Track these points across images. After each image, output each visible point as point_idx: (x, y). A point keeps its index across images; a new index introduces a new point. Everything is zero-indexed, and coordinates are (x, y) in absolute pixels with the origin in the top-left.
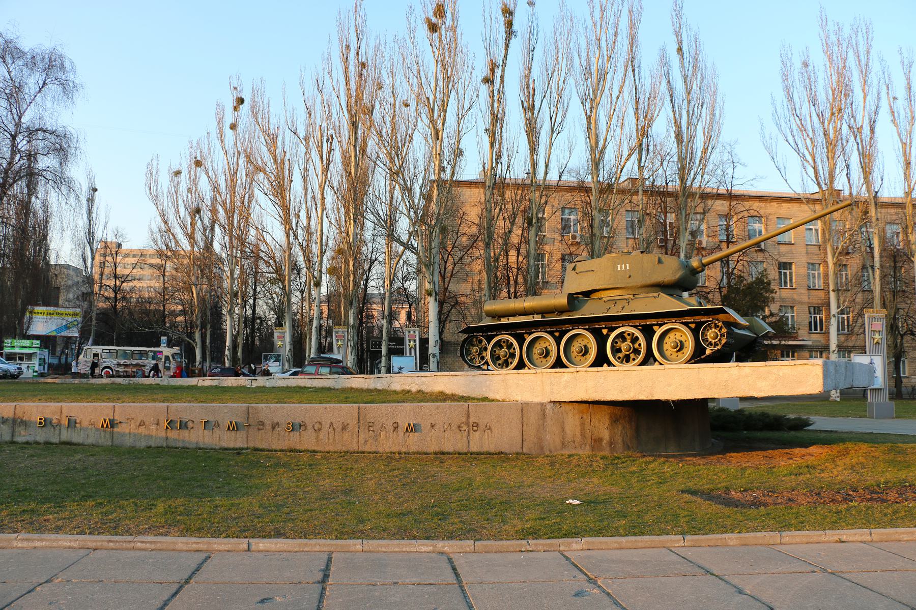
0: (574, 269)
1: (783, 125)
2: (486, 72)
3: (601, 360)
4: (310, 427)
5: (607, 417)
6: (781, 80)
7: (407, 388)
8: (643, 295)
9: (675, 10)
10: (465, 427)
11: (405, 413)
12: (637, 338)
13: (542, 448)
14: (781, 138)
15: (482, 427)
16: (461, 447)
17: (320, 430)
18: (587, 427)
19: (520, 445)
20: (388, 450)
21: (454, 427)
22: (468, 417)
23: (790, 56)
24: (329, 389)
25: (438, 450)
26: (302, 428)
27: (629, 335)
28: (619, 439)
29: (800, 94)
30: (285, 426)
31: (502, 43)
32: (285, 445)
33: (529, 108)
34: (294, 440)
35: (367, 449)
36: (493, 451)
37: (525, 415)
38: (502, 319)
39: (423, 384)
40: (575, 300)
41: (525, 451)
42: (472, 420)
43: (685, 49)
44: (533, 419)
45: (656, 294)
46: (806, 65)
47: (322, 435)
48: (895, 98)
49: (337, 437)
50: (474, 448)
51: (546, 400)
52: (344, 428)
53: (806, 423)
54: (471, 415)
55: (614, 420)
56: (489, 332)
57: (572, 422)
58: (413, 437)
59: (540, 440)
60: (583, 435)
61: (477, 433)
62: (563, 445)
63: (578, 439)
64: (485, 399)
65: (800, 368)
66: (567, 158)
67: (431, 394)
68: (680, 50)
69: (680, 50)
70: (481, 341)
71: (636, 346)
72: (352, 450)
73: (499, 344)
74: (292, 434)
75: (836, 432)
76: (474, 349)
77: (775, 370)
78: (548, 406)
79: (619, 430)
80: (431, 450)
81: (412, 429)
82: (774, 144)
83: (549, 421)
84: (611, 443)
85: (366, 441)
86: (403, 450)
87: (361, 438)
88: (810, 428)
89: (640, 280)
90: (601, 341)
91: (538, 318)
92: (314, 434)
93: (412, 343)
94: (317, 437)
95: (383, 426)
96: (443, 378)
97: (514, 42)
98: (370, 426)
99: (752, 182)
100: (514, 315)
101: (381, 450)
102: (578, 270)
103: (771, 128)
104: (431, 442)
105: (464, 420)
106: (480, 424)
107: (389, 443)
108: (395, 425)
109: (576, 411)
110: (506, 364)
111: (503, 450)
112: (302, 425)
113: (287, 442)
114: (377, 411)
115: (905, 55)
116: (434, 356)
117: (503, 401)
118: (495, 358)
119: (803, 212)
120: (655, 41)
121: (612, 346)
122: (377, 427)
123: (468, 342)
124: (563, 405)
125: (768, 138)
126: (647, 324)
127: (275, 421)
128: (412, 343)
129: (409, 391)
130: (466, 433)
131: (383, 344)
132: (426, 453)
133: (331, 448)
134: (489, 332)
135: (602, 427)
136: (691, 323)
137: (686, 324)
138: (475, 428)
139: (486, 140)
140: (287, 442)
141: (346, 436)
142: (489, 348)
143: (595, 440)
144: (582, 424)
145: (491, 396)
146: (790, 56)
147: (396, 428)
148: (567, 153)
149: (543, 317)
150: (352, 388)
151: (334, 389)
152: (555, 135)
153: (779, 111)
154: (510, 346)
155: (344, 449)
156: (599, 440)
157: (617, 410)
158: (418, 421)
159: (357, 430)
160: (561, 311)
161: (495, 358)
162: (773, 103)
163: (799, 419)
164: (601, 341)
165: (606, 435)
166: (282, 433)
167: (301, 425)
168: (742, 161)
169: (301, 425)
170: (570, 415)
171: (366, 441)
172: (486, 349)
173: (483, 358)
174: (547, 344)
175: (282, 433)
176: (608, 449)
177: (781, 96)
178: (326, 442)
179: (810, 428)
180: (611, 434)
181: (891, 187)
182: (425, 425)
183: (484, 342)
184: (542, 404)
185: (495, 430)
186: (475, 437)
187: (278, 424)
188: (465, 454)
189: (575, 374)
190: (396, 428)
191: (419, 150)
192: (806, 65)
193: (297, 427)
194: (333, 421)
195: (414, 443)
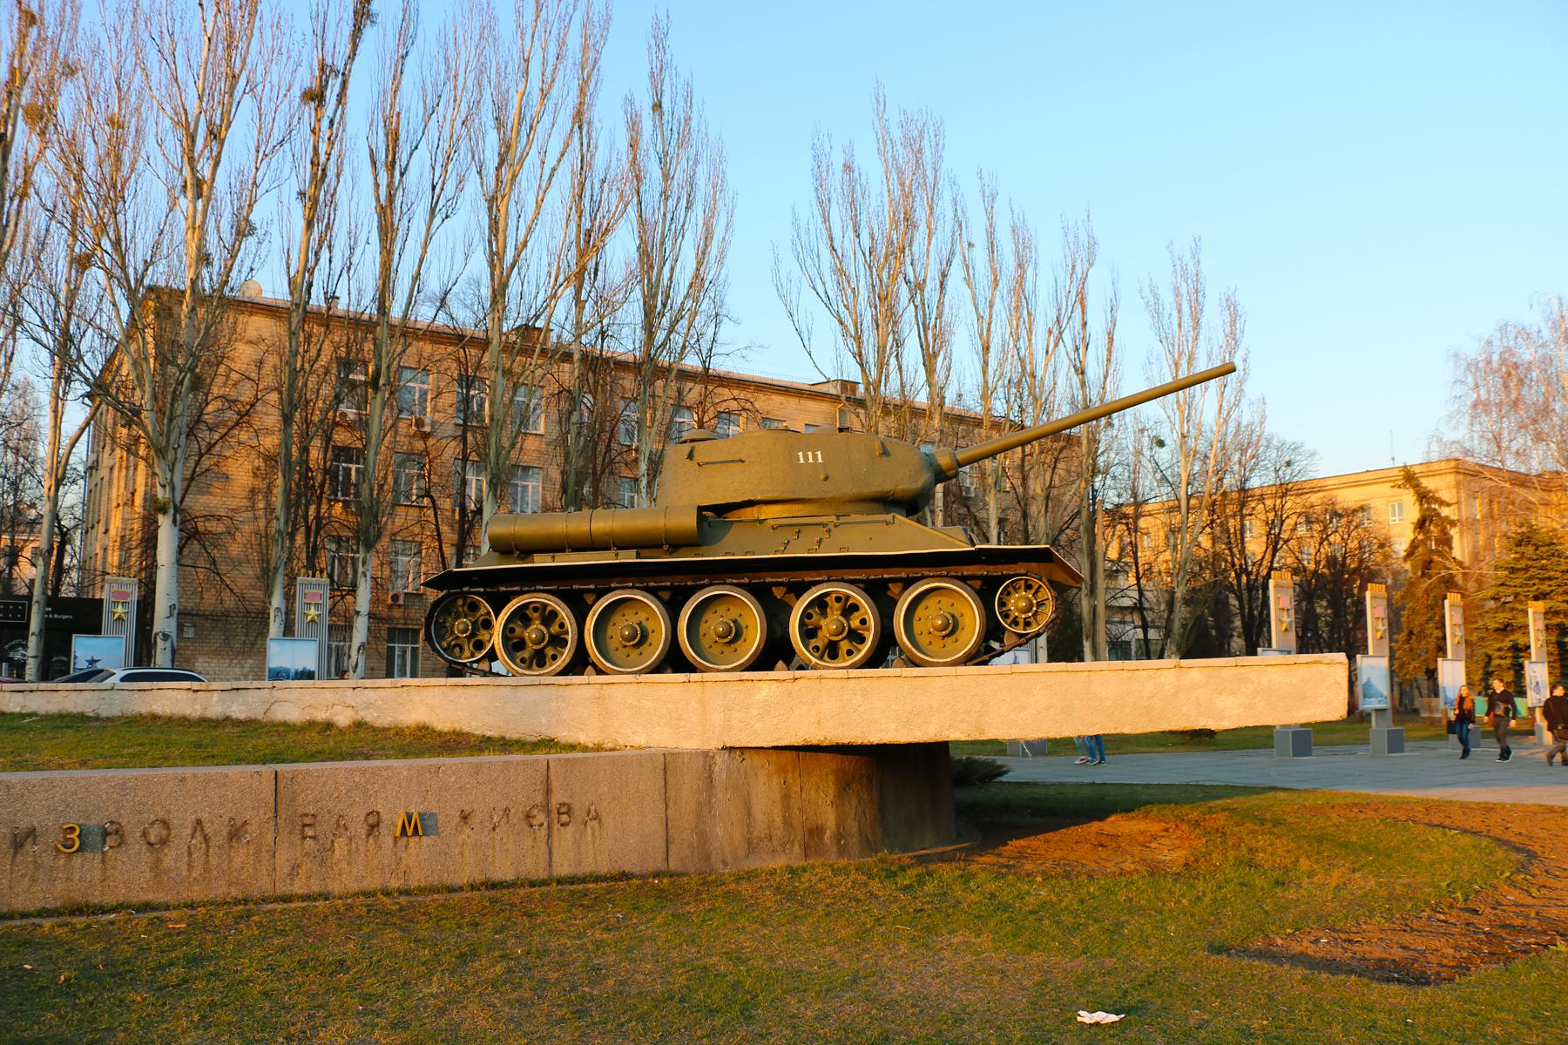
0: (690, 456)
1: (809, 262)
2: (306, 78)
3: (775, 653)
4: (134, 836)
5: (831, 778)
6: (812, 188)
7: (321, 716)
8: (854, 517)
9: (655, 37)
10: (541, 817)
11: (398, 785)
12: (855, 608)
13: (708, 857)
14: (806, 283)
15: (579, 814)
16: (533, 866)
17: (164, 842)
18: (795, 804)
19: (661, 855)
20: (354, 887)
21: (517, 818)
22: (548, 791)
23: (827, 149)
24: (82, 718)
25: (480, 878)
26: (111, 841)
27: (838, 599)
28: (852, 826)
29: (837, 215)
30: (55, 838)
31: (347, 30)
32: (53, 893)
33: (390, 161)
34: (84, 878)
35: (298, 888)
36: (604, 871)
37: (671, 781)
38: (537, 557)
39: (369, 705)
40: (716, 516)
41: (672, 866)
42: (557, 798)
43: (666, 105)
44: (687, 785)
45: (889, 517)
46: (848, 168)
47: (169, 858)
48: (970, 245)
49: (214, 861)
50: (563, 868)
51: (713, 744)
52: (235, 834)
53: (1000, 771)
54: (555, 785)
55: (844, 786)
56: (497, 587)
57: (765, 790)
58: (419, 848)
59: (704, 838)
60: (787, 822)
61: (570, 830)
62: (751, 847)
63: (778, 832)
64: (549, 744)
65: (1303, 669)
66: (446, 273)
67: (399, 732)
68: (657, 106)
69: (657, 106)
70: (474, 607)
71: (855, 623)
72: (257, 894)
73: (521, 615)
74: (77, 861)
75: (1035, 784)
76: (461, 625)
77: (1253, 674)
78: (718, 759)
79: (851, 808)
80: (463, 877)
81: (415, 827)
82: (794, 291)
83: (720, 795)
84: (839, 836)
85: (295, 868)
86: (394, 884)
87: (281, 859)
88: (1004, 779)
89: (848, 488)
90: (776, 615)
91: (628, 557)
92: (147, 857)
93: (120, 609)
94: (157, 869)
95: (340, 825)
96: (425, 692)
97: (369, 33)
98: (305, 824)
99: (745, 353)
100: (561, 550)
101: (335, 887)
102: (698, 457)
103: (789, 264)
104: (461, 858)
105: (539, 798)
106: (576, 806)
107: (357, 869)
108: (372, 820)
109: (773, 768)
110: (540, 659)
111: (627, 868)
112: (111, 834)
113: (60, 886)
114: (323, 781)
115: (986, 181)
116: (166, 637)
117: (599, 748)
118: (514, 645)
119: (817, 412)
120: (622, 83)
121: (802, 624)
122: (324, 828)
123: (440, 614)
124: (747, 754)
125: (784, 281)
126: (882, 578)
127: (24, 824)
128: (120, 609)
129: (329, 725)
130: (543, 832)
131: (35, 609)
132: (452, 890)
133: (196, 893)
134: (497, 587)
135: (822, 802)
136: (664, 589)
137: (963, 579)
138: (564, 818)
139: (298, 214)
140: (60, 886)
141: (241, 855)
142: (499, 624)
143: (811, 832)
144: (786, 797)
145: (564, 735)
146: (827, 149)
147: (373, 828)
148: (460, 257)
149: (638, 556)
150: (155, 717)
151: (97, 718)
152: (437, 220)
153: (804, 237)
154: (549, 617)
155: (235, 892)
156: (817, 831)
157: (848, 762)
158: (431, 806)
159: (270, 837)
160: (676, 543)
161: (514, 645)
162: (795, 222)
163: (991, 764)
164: (776, 615)
165: (829, 818)
166: (47, 860)
167: (106, 834)
168: (734, 315)
169: (106, 834)
170: (762, 778)
171: (295, 868)
172: (488, 625)
173: (479, 645)
174: (642, 616)
175: (47, 860)
176: (834, 849)
177: (809, 211)
178: (186, 877)
179: (1004, 779)
180: (838, 817)
181: (964, 384)
182: (448, 818)
183: (485, 607)
184: (706, 754)
185: (608, 821)
186: (565, 838)
187: (32, 833)
188: (544, 883)
189: (788, 685)
190: (373, 828)
191: (150, 204)
192: (848, 168)
193: (94, 839)
194: (204, 816)
195: (420, 863)
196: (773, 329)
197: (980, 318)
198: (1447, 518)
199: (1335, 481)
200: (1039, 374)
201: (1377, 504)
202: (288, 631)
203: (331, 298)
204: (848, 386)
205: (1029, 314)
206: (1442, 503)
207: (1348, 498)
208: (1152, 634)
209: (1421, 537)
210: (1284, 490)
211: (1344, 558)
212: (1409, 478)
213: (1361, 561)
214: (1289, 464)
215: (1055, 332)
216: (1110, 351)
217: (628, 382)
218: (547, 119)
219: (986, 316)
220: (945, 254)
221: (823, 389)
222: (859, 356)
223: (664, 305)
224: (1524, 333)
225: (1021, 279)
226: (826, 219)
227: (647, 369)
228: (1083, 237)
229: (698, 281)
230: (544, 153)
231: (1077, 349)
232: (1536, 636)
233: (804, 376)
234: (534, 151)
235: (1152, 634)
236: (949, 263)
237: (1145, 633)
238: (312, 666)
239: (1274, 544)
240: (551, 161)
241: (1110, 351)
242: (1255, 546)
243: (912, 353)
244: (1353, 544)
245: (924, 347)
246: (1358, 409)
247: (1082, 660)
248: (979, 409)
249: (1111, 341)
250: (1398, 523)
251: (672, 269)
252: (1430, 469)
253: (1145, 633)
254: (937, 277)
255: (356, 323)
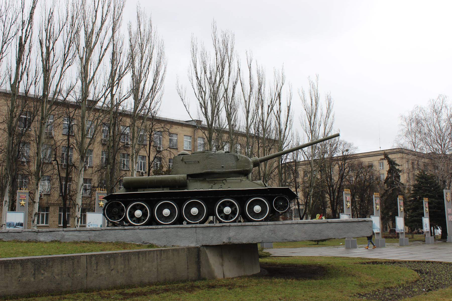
125: (180, 88)
152: (66, 66)
196: (177, 102)
197: (246, 101)
198: (398, 169)
199: (361, 155)
200: (265, 120)
201: (376, 164)
202: (85, 226)
203: (27, 92)
204: (199, 122)
205: (262, 100)
206: (397, 165)
207: (366, 161)
208: (301, 207)
209: (390, 176)
210: (345, 158)
211: (365, 182)
212: (386, 155)
213: (370, 183)
214: (347, 150)
215: (271, 107)
216: (288, 113)
217: (128, 121)
218: (103, 32)
219: (248, 101)
220: (235, 80)
221: (190, 123)
222: (206, 114)
223: (142, 96)
224: (421, 109)
225: (260, 90)
226: (195, 67)
227: (134, 116)
228: (281, 75)
229: (153, 89)
230: (102, 44)
231: (278, 112)
232: (426, 210)
233: (183, 117)
234: (99, 42)
235: (301, 207)
236: (236, 82)
237: (299, 207)
238: (22, 221)
239: (342, 177)
240: (104, 47)
241: (288, 113)
242: (336, 178)
243: (223, 114)
244: (367, 177)
245: (227, 111)
246: (372, 126)
247: (279, 221)
248: (245, 132)
249: (289, 110)
250: (383, 170)
251: (144, 85)
252: (393, 151)
253: (299, 207)
254: (232, 88)
255: (36, 99)
